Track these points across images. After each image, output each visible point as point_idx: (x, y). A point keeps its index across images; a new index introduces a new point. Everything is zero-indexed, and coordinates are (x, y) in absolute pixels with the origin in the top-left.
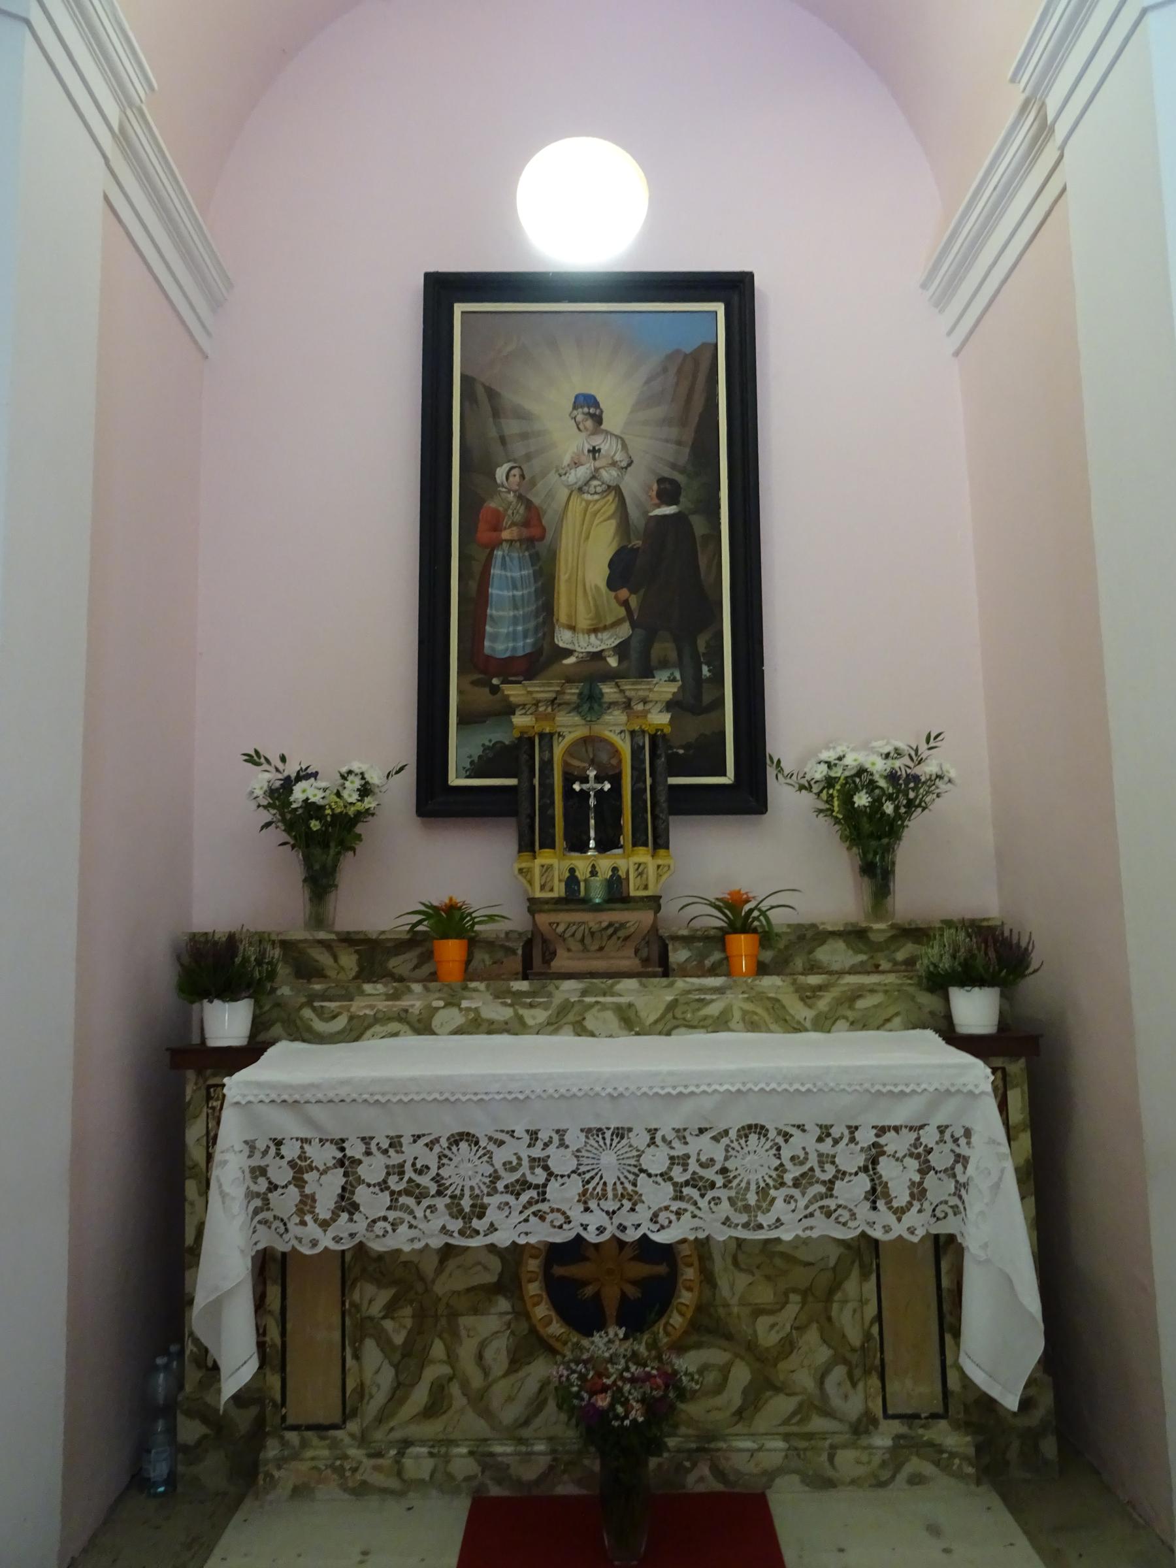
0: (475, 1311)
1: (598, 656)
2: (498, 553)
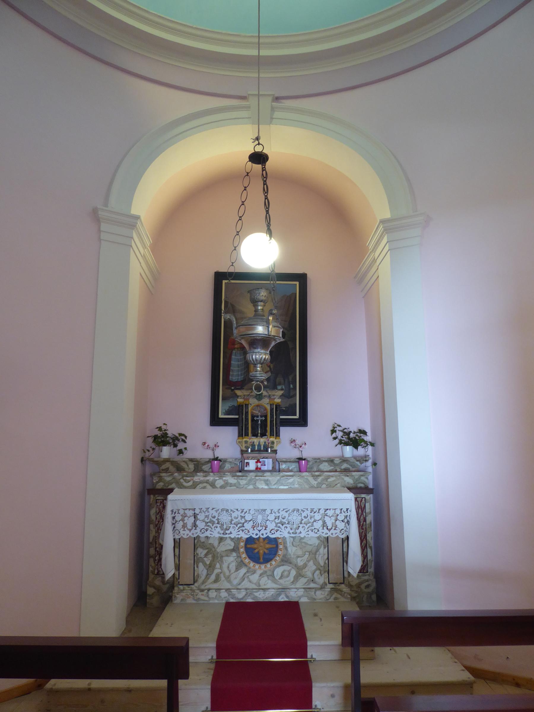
0: (227, 556)
2: (234, 352)
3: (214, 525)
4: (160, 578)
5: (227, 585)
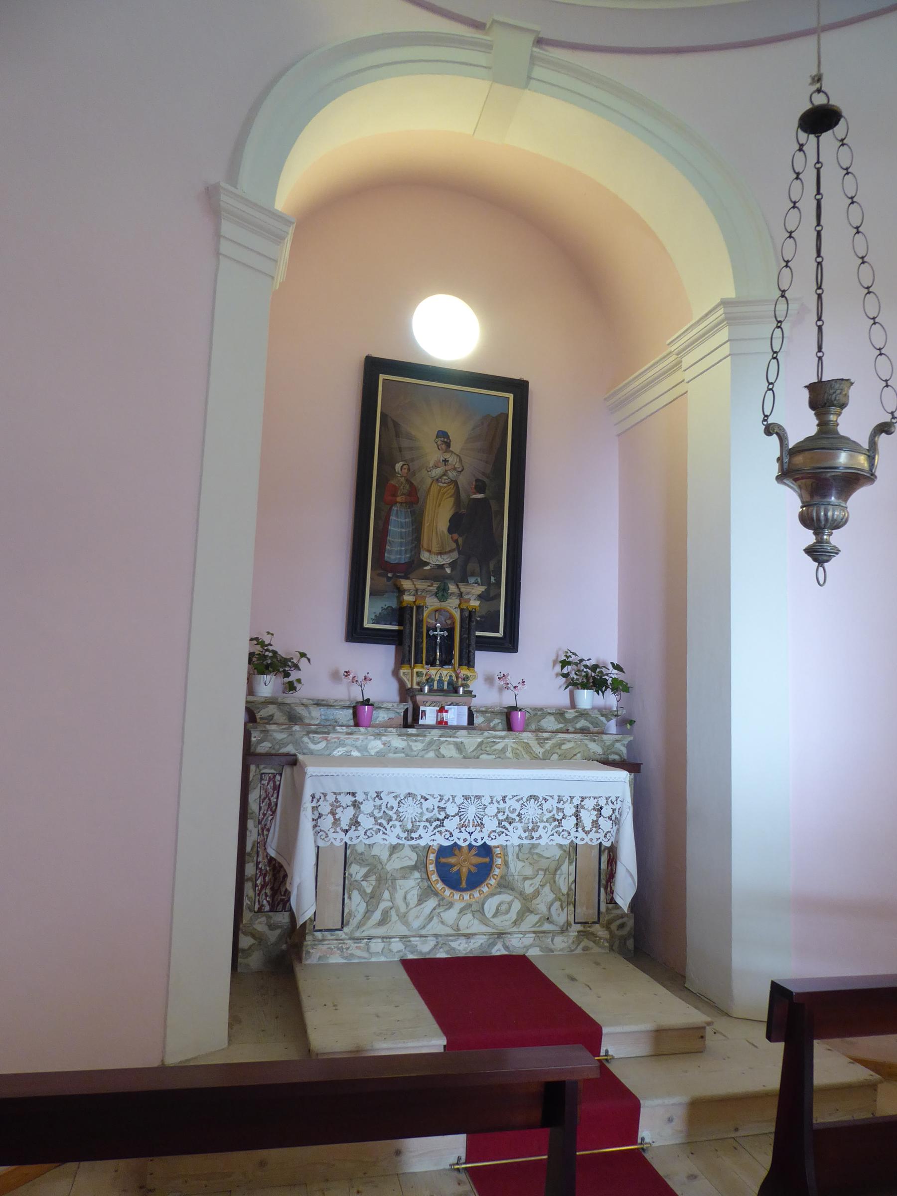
0: (404, 878)
1: (441, 567)
2: (395, 508)
3: (391, 823)
4: (264, 919)
5: (403, 930)
